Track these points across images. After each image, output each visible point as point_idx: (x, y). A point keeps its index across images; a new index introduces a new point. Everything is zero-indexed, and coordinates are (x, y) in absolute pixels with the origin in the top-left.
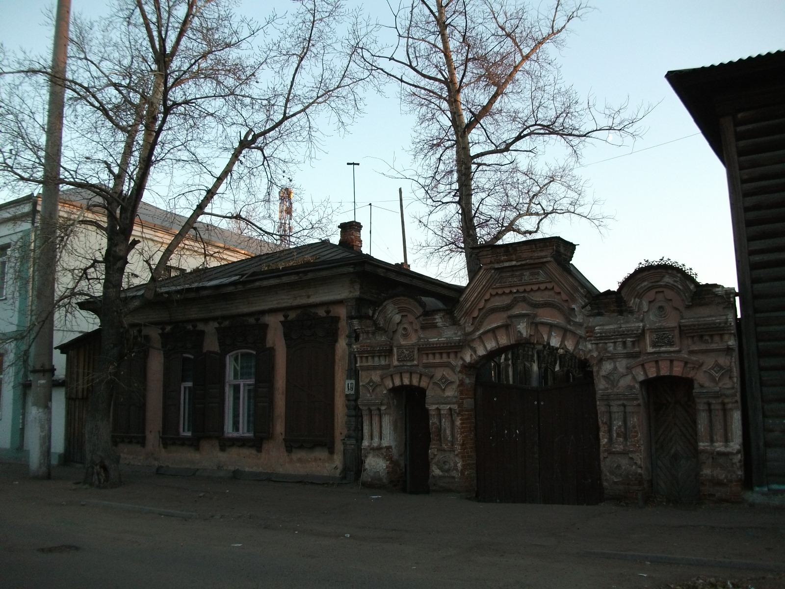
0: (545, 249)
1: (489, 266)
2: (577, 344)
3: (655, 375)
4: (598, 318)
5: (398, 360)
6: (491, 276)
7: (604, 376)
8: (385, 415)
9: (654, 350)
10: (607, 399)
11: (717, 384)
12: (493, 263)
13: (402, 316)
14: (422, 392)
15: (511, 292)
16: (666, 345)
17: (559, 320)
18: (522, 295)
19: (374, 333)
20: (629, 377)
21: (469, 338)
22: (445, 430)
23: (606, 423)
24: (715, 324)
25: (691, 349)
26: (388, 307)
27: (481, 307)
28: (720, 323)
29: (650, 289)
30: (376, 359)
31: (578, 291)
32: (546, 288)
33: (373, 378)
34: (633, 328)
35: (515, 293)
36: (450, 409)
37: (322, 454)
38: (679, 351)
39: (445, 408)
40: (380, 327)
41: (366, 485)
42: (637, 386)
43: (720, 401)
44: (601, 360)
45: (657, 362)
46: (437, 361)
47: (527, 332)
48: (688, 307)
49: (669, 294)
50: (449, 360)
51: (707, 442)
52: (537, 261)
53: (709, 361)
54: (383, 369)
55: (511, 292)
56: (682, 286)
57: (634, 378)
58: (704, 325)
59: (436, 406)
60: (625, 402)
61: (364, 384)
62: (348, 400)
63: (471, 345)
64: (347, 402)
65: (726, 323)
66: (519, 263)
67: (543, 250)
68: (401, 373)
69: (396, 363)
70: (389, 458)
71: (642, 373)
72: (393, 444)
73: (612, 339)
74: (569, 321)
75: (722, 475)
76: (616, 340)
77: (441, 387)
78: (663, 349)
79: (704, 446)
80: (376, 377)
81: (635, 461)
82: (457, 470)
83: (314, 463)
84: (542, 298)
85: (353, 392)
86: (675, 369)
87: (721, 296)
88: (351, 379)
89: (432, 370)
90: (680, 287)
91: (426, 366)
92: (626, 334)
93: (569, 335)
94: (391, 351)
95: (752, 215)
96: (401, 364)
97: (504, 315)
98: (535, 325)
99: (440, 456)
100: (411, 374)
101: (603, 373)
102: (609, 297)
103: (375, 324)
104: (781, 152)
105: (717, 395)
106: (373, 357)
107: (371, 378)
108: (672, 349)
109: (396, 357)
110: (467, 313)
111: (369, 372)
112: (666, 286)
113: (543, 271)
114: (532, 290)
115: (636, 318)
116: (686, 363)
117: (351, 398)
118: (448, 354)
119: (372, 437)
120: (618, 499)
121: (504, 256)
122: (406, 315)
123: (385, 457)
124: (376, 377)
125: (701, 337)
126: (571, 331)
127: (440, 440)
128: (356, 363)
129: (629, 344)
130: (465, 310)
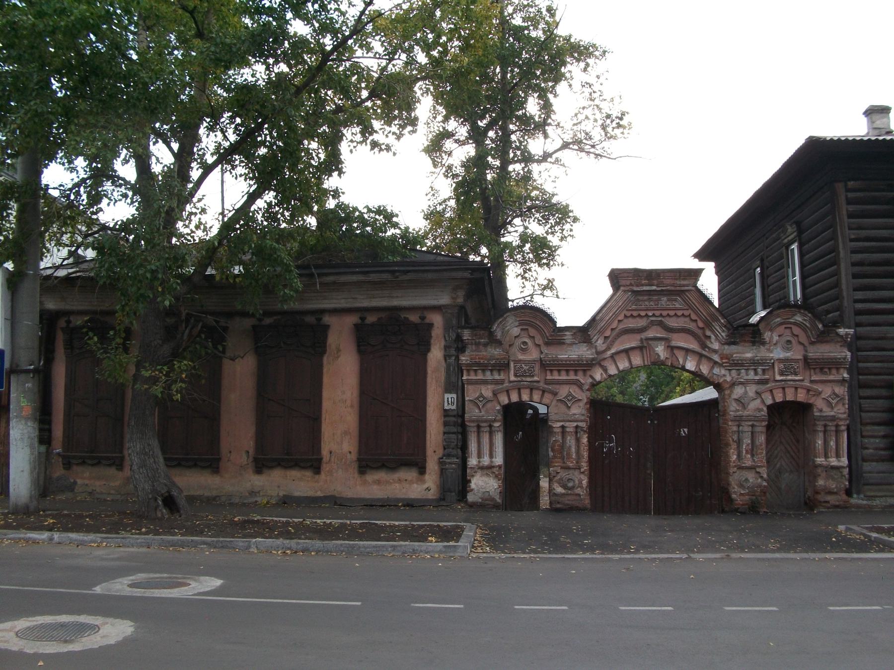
3: (781, 400)
4: (733, 347)
5: (516, 375)
7: (736, 400)
9: (782, 378)
10: (739, 420)
11: (832, 408)
12: (633, 286)
13: (522, 329)
15: (647, 315)
16: (792, 374)
17: (694, 345)
18: (660, 319)
19: (485, 345)
20: (758, 401)
22: (570, 446)
23: (736, 442)
24: (836, 359)
25: (812, 379)
28: (840, 359)
29: (781, 324)
30: (488, 373)
31: (718, 320)
33: (483, 392)
35: (651, 316)
36: (577, 427)
37: (409, 474)
38: (802, 381)
39: (570, 426)
41: (472, 505)
42: (765, 409)
43: (835, 423)
44: (733, 385)
45: (784, 388)
48: (812, 343)
49: (797, 331)
52: (678, 288)
53: (827, 391)
54: (495, 384)
55: (647, 315)
56: (811, 325)
57: (763, 402)
58: (828, 359)
59: (562, 424)
60: (755, 423)
62: (445, 416)
65: (844, 359)
68: (519, 389)
69: (512, 378)
71: (770, 397)
74: (704, 346)
75: (833, 485)
78: (789, 378)
80: (487, 392)
82: (582, 487)
83: (397, 485)
85: (454, 407)
86: (799, 395)
87: (842, 336)
88: (450, 393)
89: (558, 386)
90: (807, 324)
91: (547, 382)
93: (704, 360)
95: (857, 269)
96: (519, 379)
97: (638, 337)
98: (672, 349)
99: (563, 474)
100: (531, 390)
101: (734, 396)
102: (748, 328)
103: (491, 334)
104: (891, 220)
105: (833, 419)
106: (483, 371)
109: (512, 372)
110: (601, 332)
111: (477, 386)
112: (795, 324)
113: (680, 297)
114: (668, 315)
115: (767, 349)
116: (808, 391)
117: (451, 413)
119: (479, 456)
120: (753, 509)
124: (487, 392)
128: (462, 376)
129: (760, 371)
130: (599, 328)
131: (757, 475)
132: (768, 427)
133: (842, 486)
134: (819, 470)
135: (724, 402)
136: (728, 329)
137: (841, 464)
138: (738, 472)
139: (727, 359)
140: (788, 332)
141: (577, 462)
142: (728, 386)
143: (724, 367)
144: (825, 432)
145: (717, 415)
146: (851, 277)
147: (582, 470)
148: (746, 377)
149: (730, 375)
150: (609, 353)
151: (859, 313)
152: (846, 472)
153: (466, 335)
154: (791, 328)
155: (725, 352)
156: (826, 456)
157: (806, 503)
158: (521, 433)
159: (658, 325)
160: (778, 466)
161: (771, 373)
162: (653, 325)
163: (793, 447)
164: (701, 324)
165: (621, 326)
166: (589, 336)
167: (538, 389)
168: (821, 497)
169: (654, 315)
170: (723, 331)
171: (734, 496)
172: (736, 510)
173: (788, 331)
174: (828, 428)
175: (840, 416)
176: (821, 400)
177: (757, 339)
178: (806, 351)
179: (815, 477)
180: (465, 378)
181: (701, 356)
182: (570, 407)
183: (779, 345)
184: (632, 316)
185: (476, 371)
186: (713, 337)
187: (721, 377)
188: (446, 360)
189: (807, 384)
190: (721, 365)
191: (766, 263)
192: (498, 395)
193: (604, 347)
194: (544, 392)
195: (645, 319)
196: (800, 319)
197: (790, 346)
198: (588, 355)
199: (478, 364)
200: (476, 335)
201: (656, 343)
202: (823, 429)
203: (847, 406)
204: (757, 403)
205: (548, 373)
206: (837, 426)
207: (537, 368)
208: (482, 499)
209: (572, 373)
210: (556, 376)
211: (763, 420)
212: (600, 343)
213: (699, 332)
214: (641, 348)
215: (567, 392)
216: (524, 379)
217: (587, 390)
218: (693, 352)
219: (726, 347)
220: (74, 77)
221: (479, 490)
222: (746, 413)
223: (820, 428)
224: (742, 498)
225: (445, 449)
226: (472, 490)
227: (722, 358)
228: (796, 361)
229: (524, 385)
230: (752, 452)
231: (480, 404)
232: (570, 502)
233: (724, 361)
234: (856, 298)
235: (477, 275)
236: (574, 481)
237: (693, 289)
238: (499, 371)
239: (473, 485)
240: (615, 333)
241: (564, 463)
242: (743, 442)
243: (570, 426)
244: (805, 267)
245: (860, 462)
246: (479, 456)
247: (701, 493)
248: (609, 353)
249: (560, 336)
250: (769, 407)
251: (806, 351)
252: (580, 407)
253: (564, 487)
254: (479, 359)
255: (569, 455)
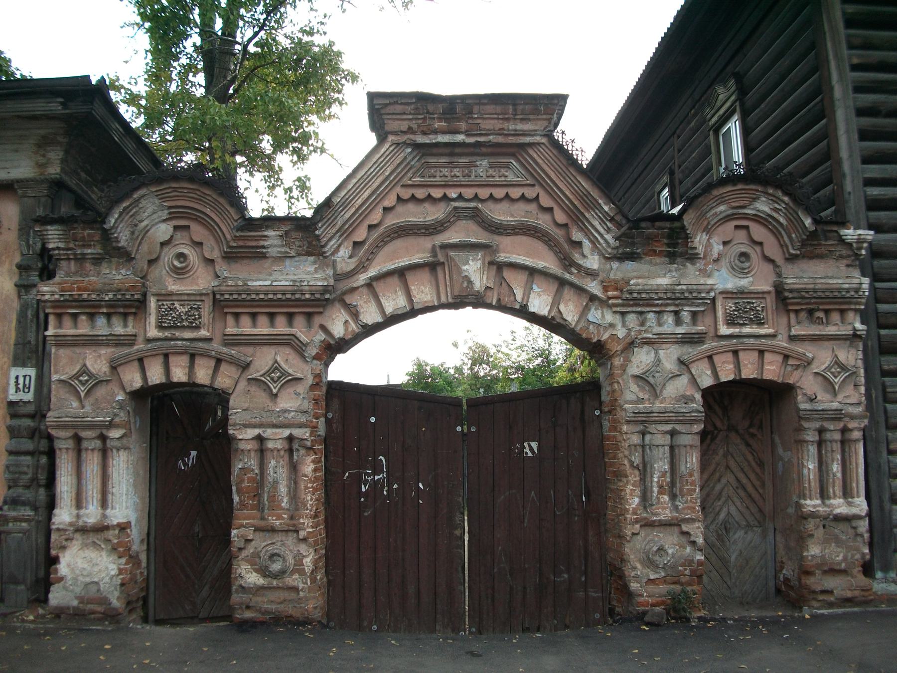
0: (532, 117)
1: (405, 138)
2: (586, 309)
3: (731, 377)
4: (629, 265)
5: (160, 327)
6: (405, 158)
8: (118, 450)
11: (835, 394)
12: (414, 133)
13: (176, 228)
14: (223, 398)
15: (445, 197)
17: (546, 261)
18: (472, 205)
19: (97, 261)
20: (684, 380)
21: (344, 286)
22: (276, 482)
23: (637, 468)
24: (840, 290)
25: (793, 332)
26: (143, 203)
27: (375, 222)
30: (101, 321)
32: (523, 197)
33: (89, 364)
34: (702, 287)
36: (290, 439)
38: (773, 336)
39: (276, 438)
40: (119, 248)
42: (698, 397)
43: (841, 425)
44: (630, 345)
45: (735, 353)
46: (266, 330)
47: (481, 280)
48: (791, 259)
49: (759, 232)
50: (293, 331)
51: (817, 499)
52: (511, 140)
53: (822, 357)
54: (117, 345)
55: (445, 197)
57: (694, 381)
59: (256, 432)
60: (678, 427)
61: (63, 377)
62: (13, 416)
63: (348, 302)
64: (8, 419)
65: (857, 291)
66: (471, 140)
67: (529, 120)
68: (166, 356)
70: (120, 550)
71: (709, 372)
72: (133, 518)
73: (657, 305)
74: (568, 263)
75: (838, 556)
76: (663, 309)
77: (77, 393)
78: (747, 330)
79: (814, 506)
81: (692, 539)
82: (302, 572)
84: (512, 215)
85: (29, 397)
86: (767, 367)
87: (850, 245)
88: (24, 365)
89: (249, 350)
90: (782, 220)
91: (231, 341)
92: (686, 298)
93: (567, 293)
94: (142, 304)
95: (867, 121)
96: (167, 334)
97: (427, 243)
99: (260, 543)
100: (193, 357)
101: (634, 369)
102: (658, 224)
103: (107, 237)
105: (837, 415)
106: (92, 316)
107: (85, 365)
108: (763, 331)
109: (152, 319)
110: (345, 232)
111: (78, 350)
112: (756, 219)
115: (700, 270)
116: (786, 357)
118: (290, 316)
119: (79, 503)
121: (440, 119)
122: (188, 227)
123: (114, 549)
125: (811, 312)
126: (572, 285)
127: (260, 507)
128: (46, 329)
129: (686, 316)
130: (339, 224)
131: (684, 540)
132: (704, 435)
133: (858, 556)
134: (811, 525)
135: (611, 384)
136: (619, 226)
137: (854, 511)
138: (643, 534)
139: (616, 289)
140: (742, 235)
141: (292, 518)
142: (619, 348)
143: (610, 307)
144: (820, 443)
145: (597, 413)
146: (856, 137)
147: (302, 534)
148: (657, 330)
149: (624, 324)
150: (363, 278)
151: (873, 205)
152: (863, 526)
153: (54, 237)
154: (747, 228)
155: (612, 276)
156: (824, 495)
157: (778, 591)
158: (194, 453)
159: (471, 218)
160: (722, 516)
161: (709, 320)
162: (459, 218)
163: (752, 476)
164: (561, 217)
165: (392, 220)
166: (318, 238)
167: (206, 355)
168: (817, 582)
169: (460, 197)
170: (608, 230)
171: (634, 586)
172: (641, 617)
173: (742, 234)
174: (828, 436)
175: (851, 409)
176: (811, 377)
177: (678, 249)
178: (779, 275)
179: (802, 539)
180: (50, 332)
181: (562, 283)
182: (276, 395)
183: (724, 262)
184: (413, 198)
185: (75, 316)
186: (586, 243)
187: (606, 329)
188: (19, 296)
189: (782, 342)
190: (603, 303)
191: (678, 175)
192: (120, 369)
193: (351, 264)
194: (219, 361)
195: (443, 205)
196: (766, 209)
197: (746, 265)
198: (317, 279)
199: (79, 302)
200: (75, 240)
201: (463, 254)
202: (817, 438)
203: (862, 389)
204: (681, 385)
205: (230, 320)
206: (844, 430)
207: (206, 309)
208: (81, 600)
209: (281, 321)
210: (246, 327)
211: (696, 421)
212: (344, 258)
213: (558, 234)
214: (432, 266)
215: (271, 363)
216: (178, 334)
217: (314, 358)
218: (544, 274)
219: (615, 265)
220: (465, 430)
221: (75, 579)
222: (658, 406)
223: (811, 436)
224: (651, 588)
225: (10, 488)
226: (61, 579)
227: (605, 289)
228: (761, 295)
229: (176, 346)
230: (672, 489)
231: (82, 390)
232: (273, 607)
233: (610, 293)
234: (867, 175)
235: (77, 108)
236: (284, 560)
237: (544, 140)
238: (125, 315)
239: (63, 568)
240: (375, 234)
241: (263, 518)
242: (652, 467)
243: (276, 438)
244: (753, 150)
245: (887, 505)
246: (79, 503)
247: (566, 576)
248: (363, 278)
249: (253, 238)
250: (707, 393)
251: (779, 275)
252: (298, 394)
253: (263, 572)
254: (79, 289)
255: (273, 498)
